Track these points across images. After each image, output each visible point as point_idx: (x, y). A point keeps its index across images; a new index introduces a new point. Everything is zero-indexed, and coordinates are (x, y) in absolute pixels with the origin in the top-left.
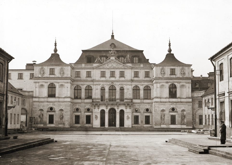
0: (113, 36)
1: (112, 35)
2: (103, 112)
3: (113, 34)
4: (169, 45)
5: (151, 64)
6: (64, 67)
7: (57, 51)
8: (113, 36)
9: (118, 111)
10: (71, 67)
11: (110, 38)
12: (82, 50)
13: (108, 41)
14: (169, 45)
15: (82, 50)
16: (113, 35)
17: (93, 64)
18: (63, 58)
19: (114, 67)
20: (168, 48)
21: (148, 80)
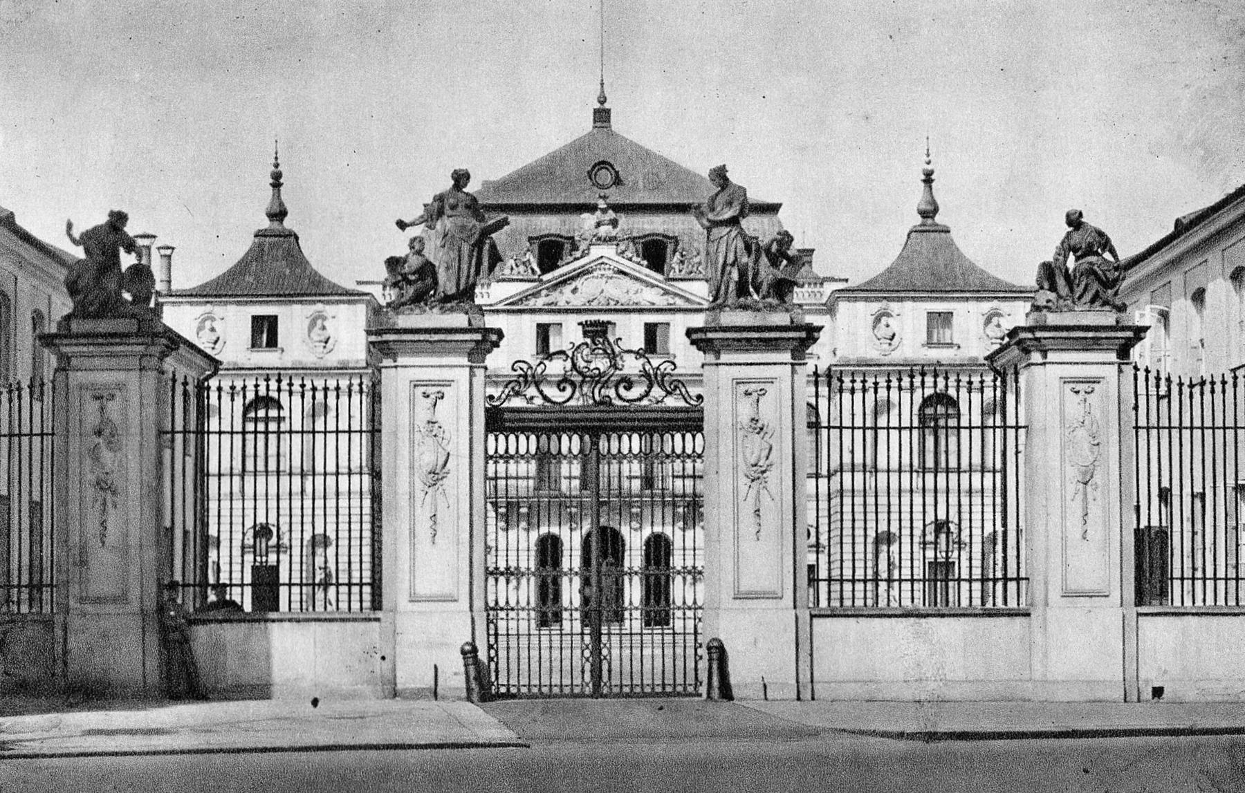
0: (602, 116)
1: (597, 106)
2: (549, 550)
3: (602, 100)
4: (271, 181)
5: (822, 284)
6: (330, 310)
7: (936, 210)
8: (602, 116)
9: (635, 540)
10: (368, 303)
11: (586, 124)
12: (780, 205)
13: (577, 147)
14: (271, 181)
15: (780, 205)
16: (607, 106)
17: (489, 285)
18: (322, 254)
19: (612, 303)
20: (916, 196)
21: (1036, 409)
